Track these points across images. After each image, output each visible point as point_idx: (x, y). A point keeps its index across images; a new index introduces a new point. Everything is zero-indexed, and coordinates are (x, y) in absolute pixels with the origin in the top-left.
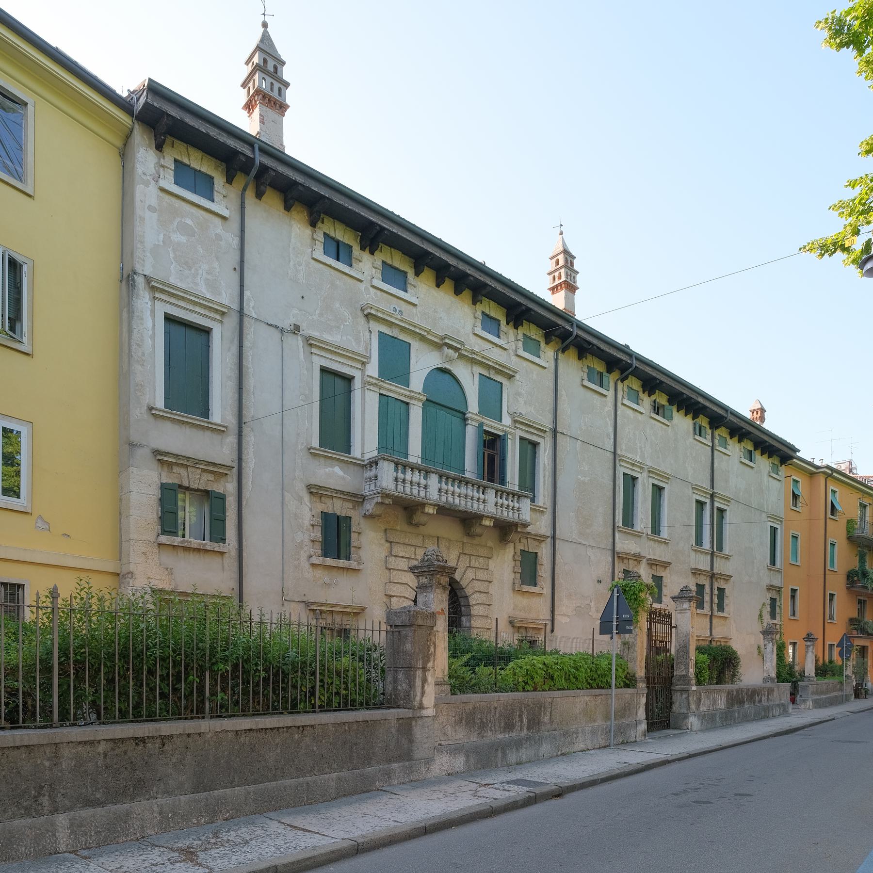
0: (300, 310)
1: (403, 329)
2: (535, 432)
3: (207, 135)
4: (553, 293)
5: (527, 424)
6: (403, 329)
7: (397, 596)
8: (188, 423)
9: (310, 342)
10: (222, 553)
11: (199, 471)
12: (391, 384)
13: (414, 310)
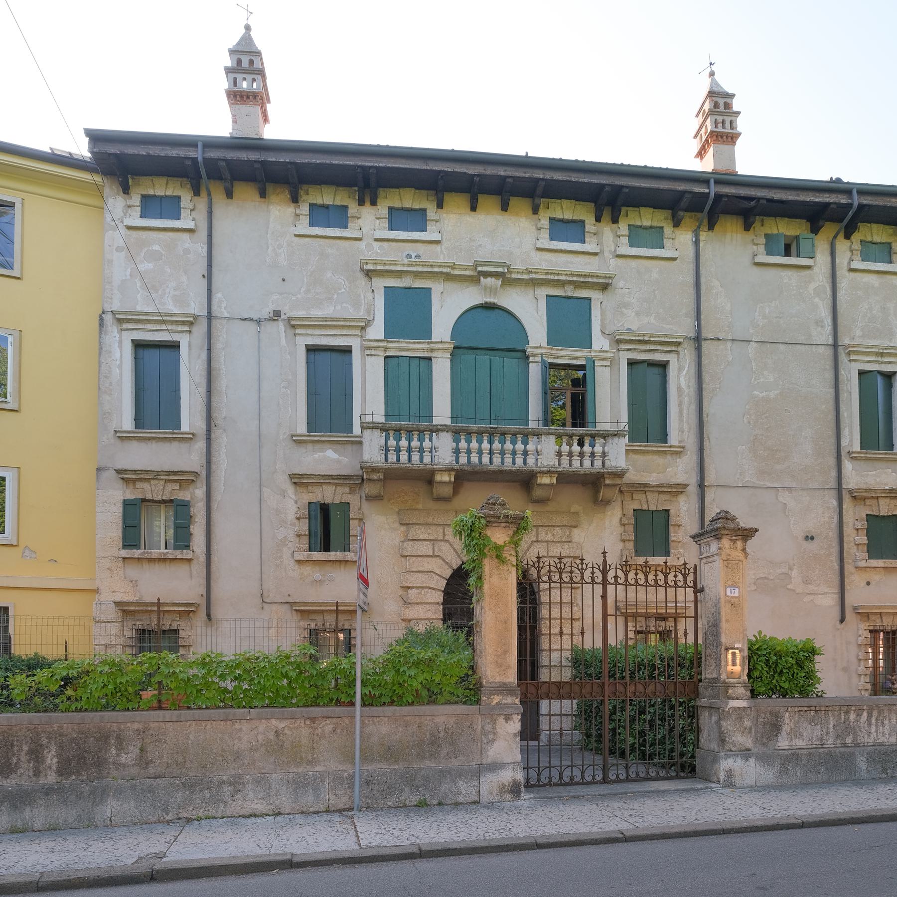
0: (281, 294)
1: (417, 275)
2: (659, 348)
3: (149, 155)
4: (702, 159)
5: (639, 341)
6: (417, 275)
7: (417, 588)
8: (154, 438)
9: (293, 325)
10: (190, 560)
11: (162, 483)
12: (398, 342)
13: (438, 248)
